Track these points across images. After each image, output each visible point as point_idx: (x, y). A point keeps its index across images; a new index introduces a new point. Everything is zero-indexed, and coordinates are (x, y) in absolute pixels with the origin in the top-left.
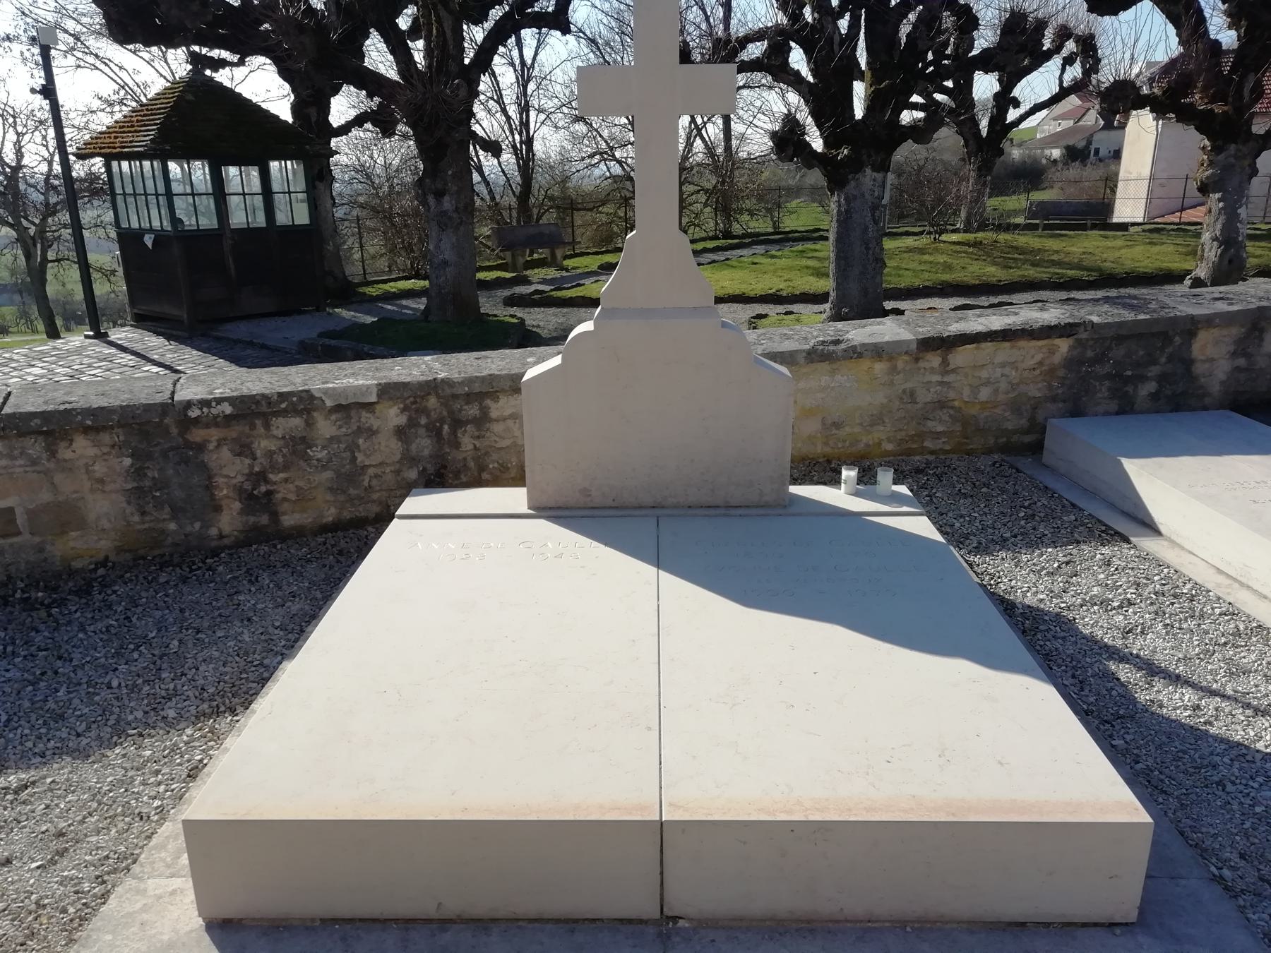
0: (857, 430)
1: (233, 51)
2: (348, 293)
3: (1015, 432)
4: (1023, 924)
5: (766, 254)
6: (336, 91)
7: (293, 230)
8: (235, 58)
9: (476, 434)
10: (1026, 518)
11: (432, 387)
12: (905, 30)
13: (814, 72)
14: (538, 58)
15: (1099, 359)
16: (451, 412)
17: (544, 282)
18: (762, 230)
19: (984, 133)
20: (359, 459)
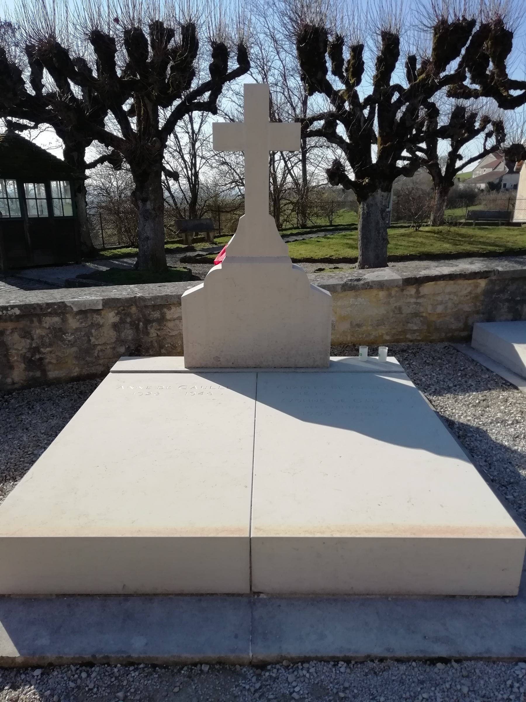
0: (370, 328)
1: (31, 120)
2: (94, 254)
4: (454, 596)
5: (325, 237)
6: (88, 144)
7: (63, 219)
8: (33, 124)
9: (158, 327)
10: (462, 376)
11: (134, 301)
12: (399, 115)
13: (350, 138)
14: (202, 128)
15: (502, 291)
16: (144, 316)
17: (203, 250)
18: (323, 224)
19: (443, 174)
20: (92, 341)
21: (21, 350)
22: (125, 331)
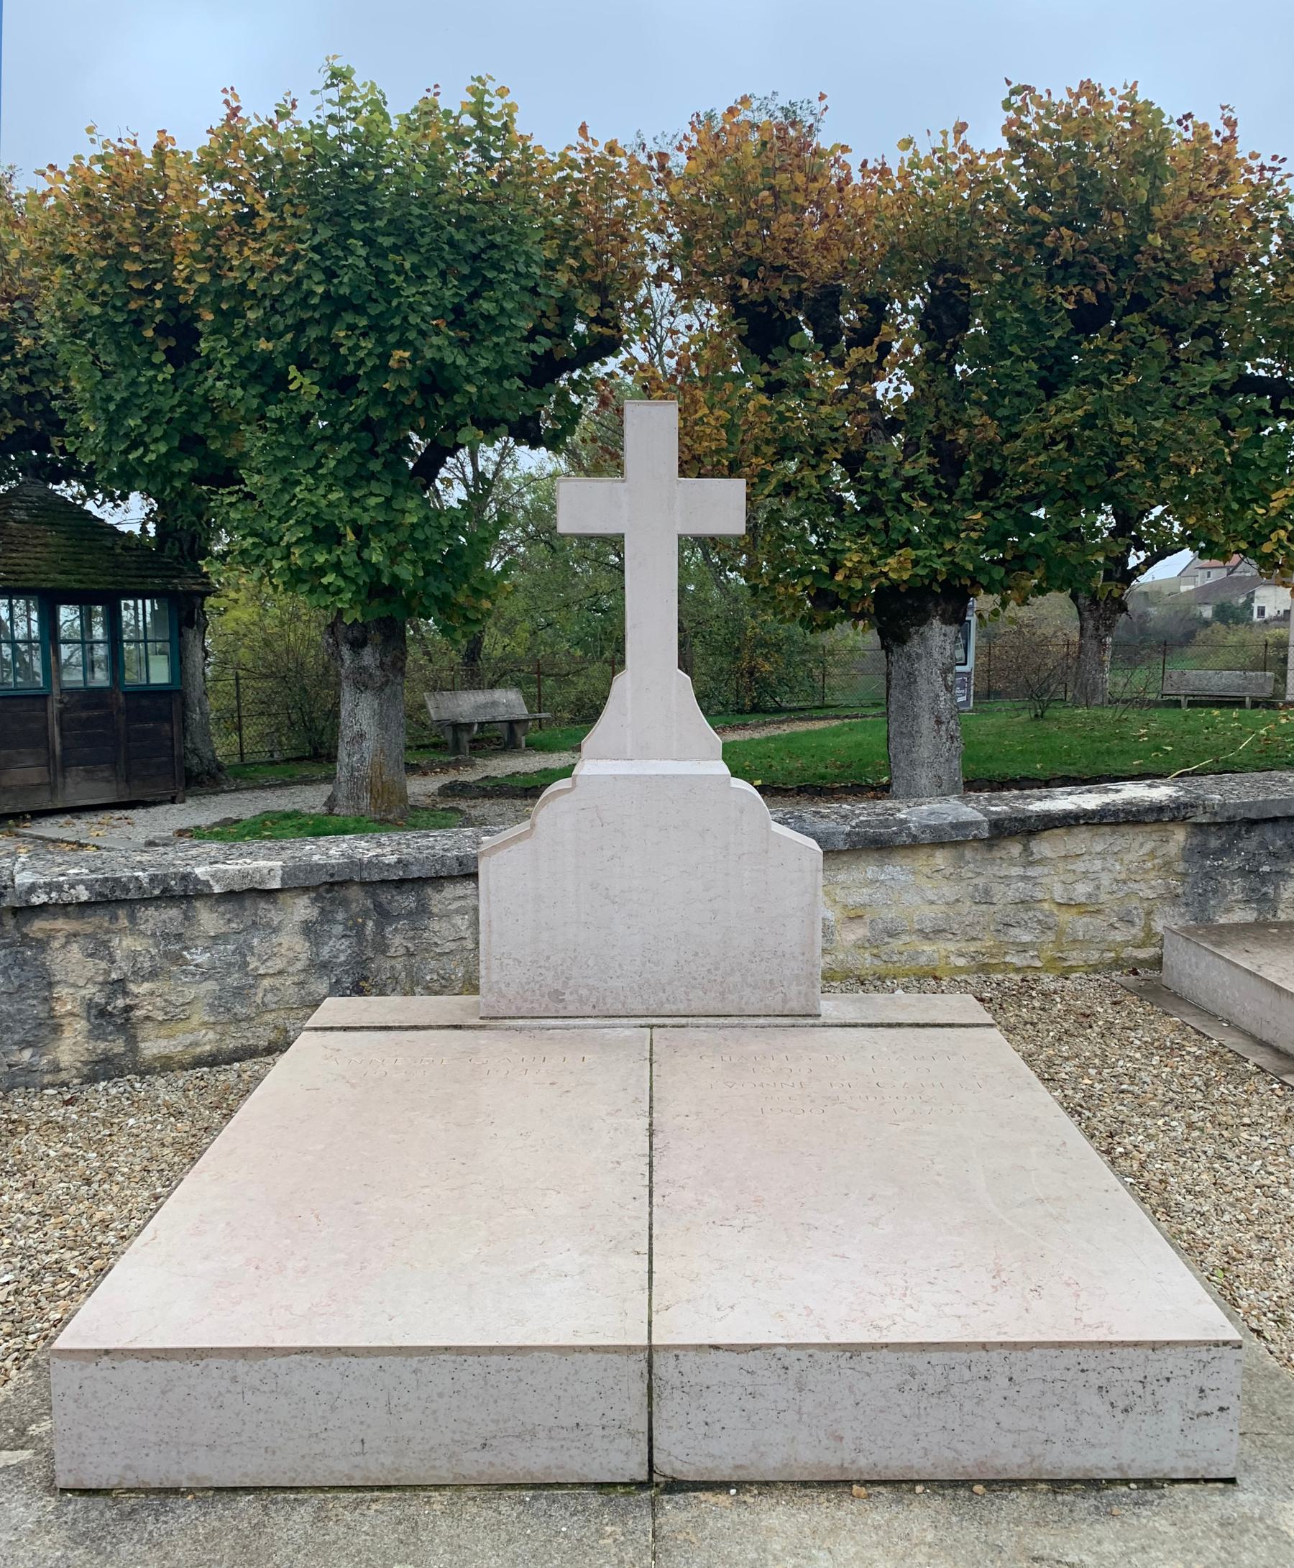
3: (1126, 944)
21: (83, 987)
22: (331, 943)
